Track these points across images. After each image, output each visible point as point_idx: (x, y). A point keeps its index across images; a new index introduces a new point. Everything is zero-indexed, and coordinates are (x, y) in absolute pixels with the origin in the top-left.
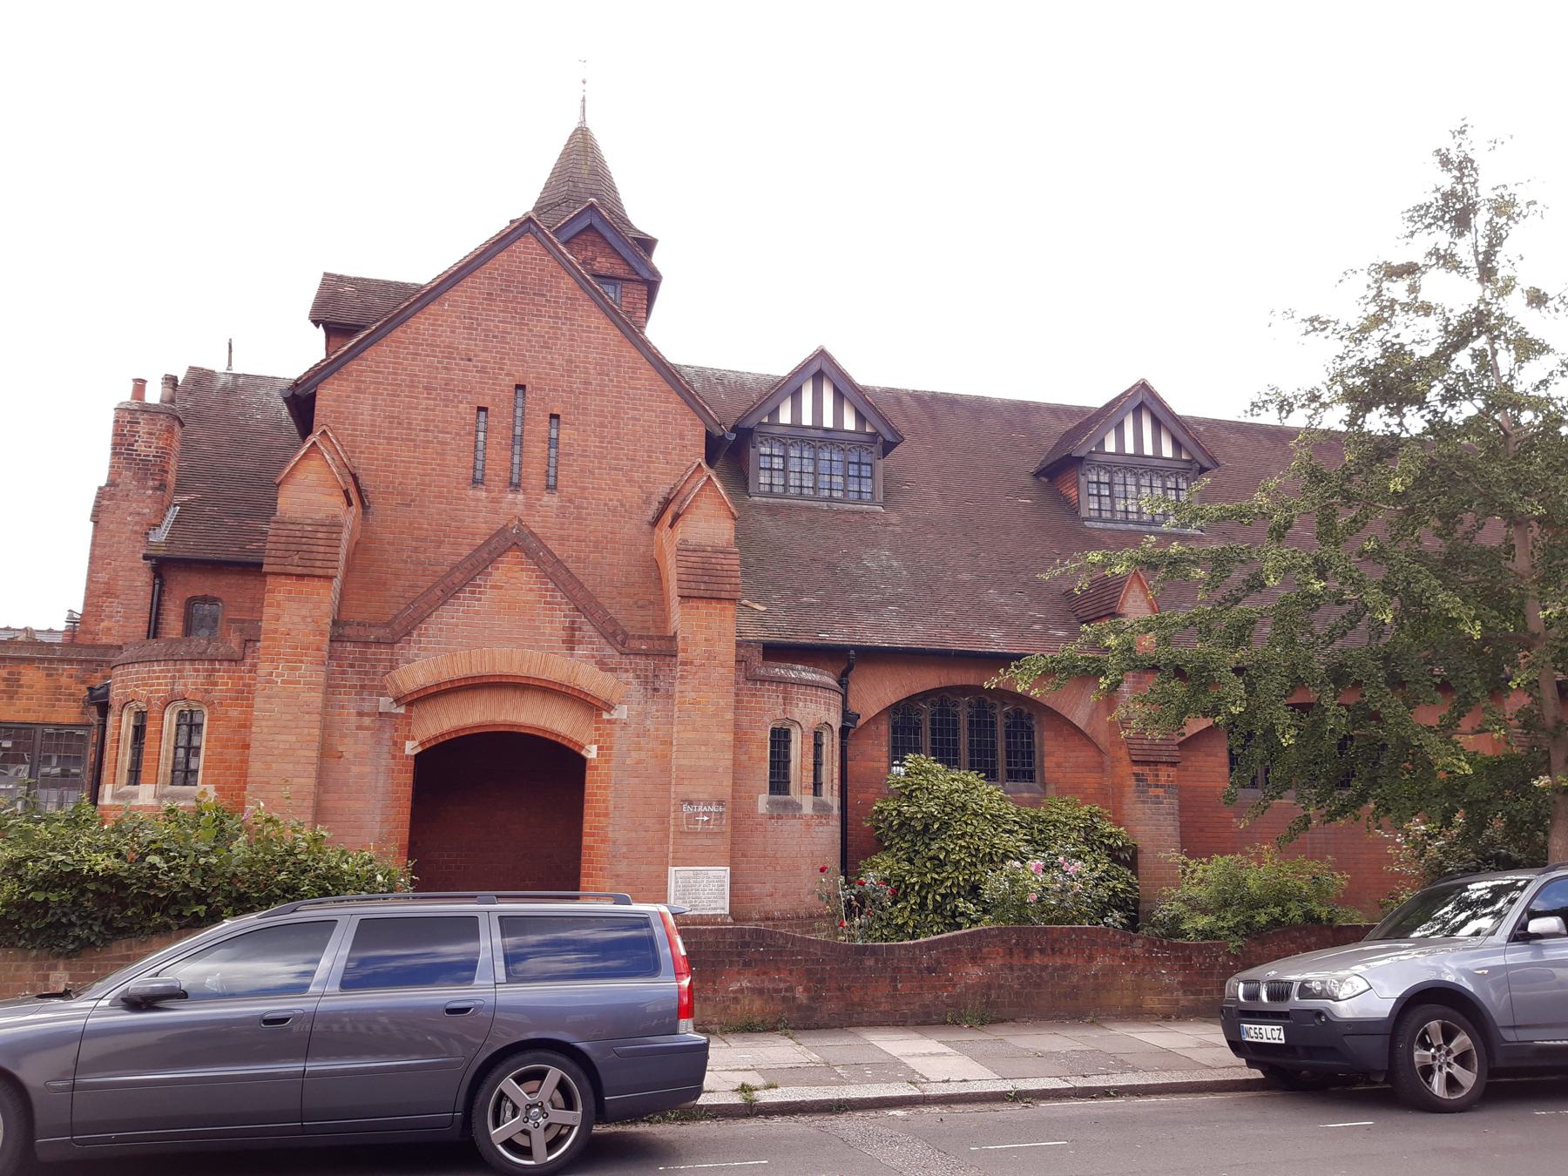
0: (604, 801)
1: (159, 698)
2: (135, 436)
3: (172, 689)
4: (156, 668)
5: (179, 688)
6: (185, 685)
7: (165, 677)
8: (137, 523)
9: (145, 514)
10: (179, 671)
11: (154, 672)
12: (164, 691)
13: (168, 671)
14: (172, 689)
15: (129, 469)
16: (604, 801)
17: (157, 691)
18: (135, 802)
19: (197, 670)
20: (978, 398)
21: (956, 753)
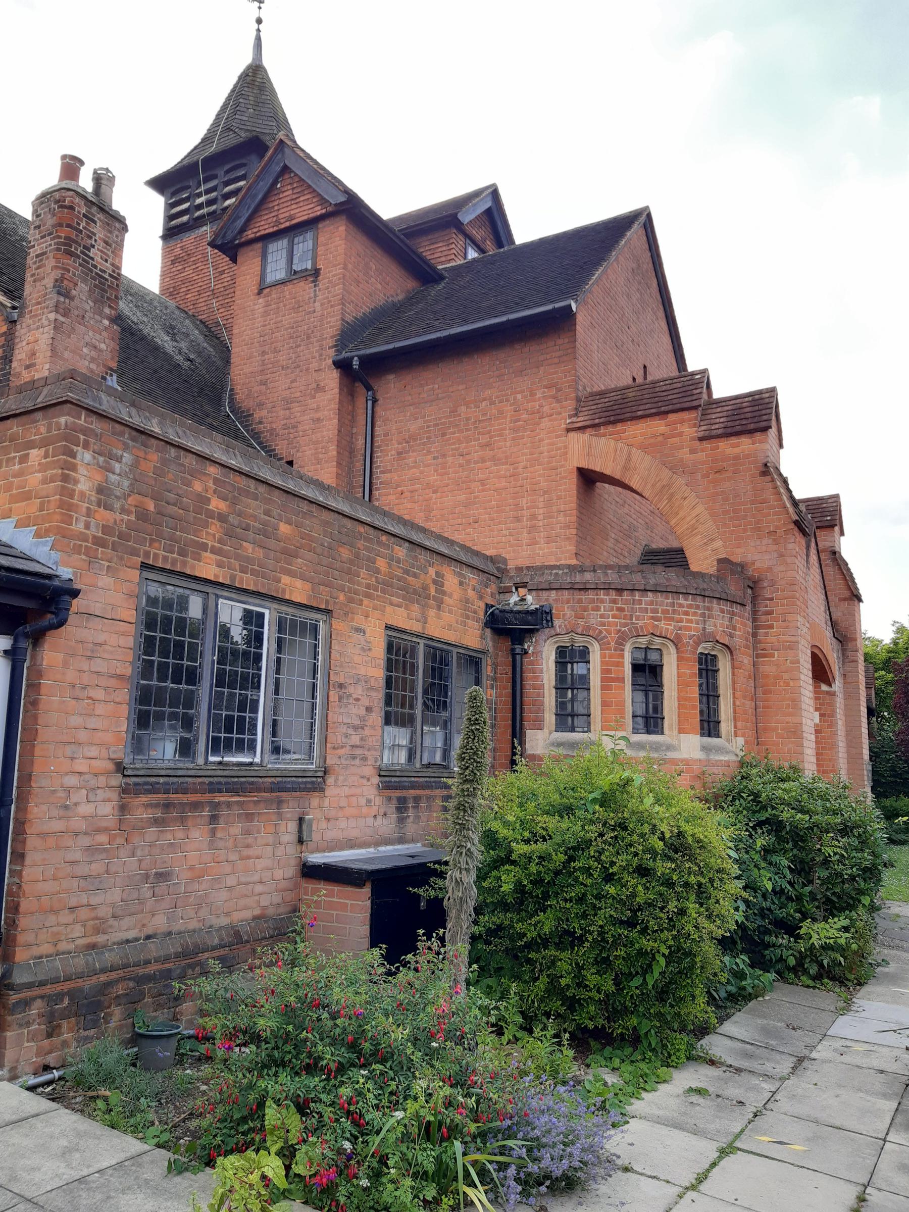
0: (830, 760)
1: (691, 637)
2: (91, 238)
3: (704, 629)
4: (682, 601)
5: (710, 628)
6: (715, 626)
7: (695, 614)
8: (93, 360)
9: (101, 351)
10: (709, 609)
11: (681, 606)
12: (696, 630)
13: (698, 607)
14: (704, 629)
15: (84, 281)
16: (830, 760)
17: (688, 629)
18: (671, 755)
19: (722, 611)
20: (541, 240)
21: (458, 657)
